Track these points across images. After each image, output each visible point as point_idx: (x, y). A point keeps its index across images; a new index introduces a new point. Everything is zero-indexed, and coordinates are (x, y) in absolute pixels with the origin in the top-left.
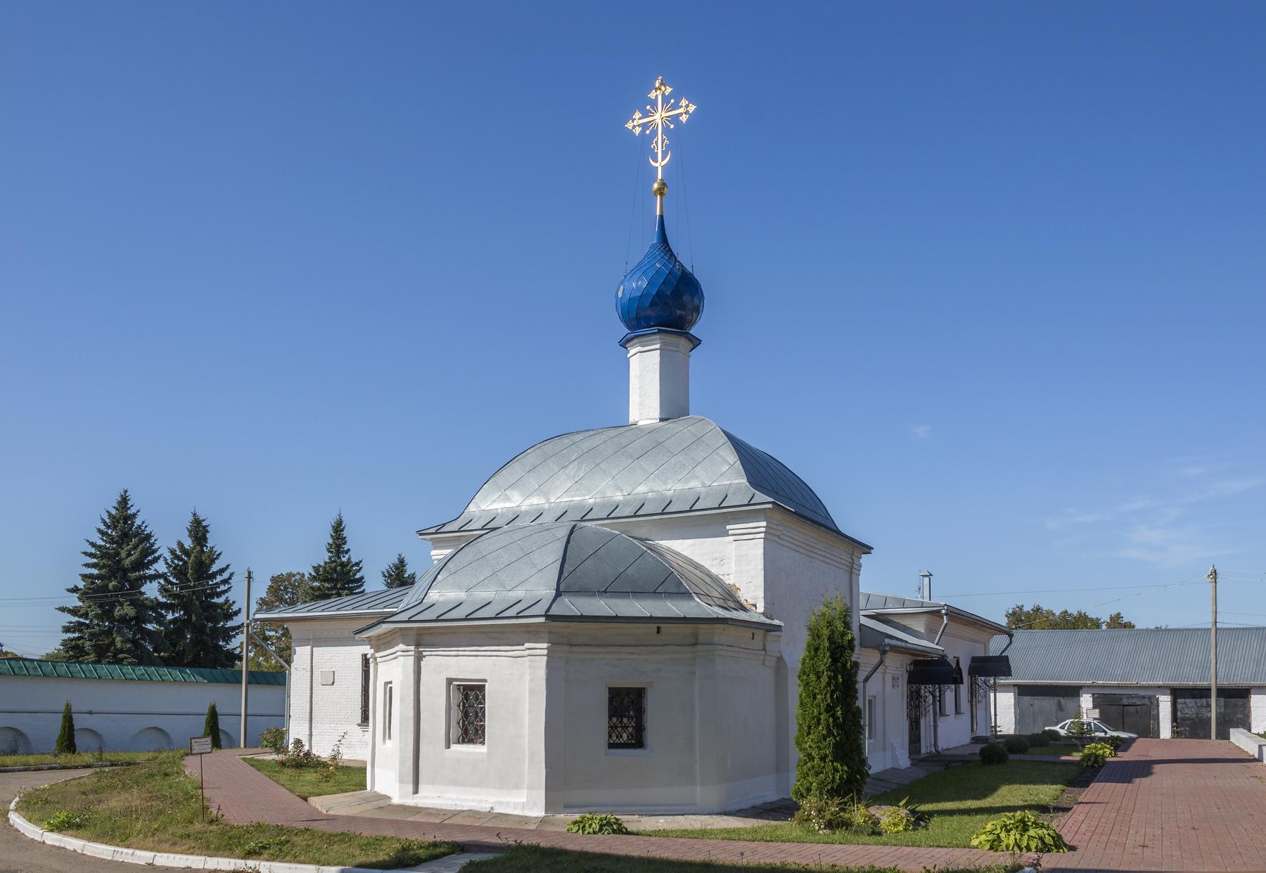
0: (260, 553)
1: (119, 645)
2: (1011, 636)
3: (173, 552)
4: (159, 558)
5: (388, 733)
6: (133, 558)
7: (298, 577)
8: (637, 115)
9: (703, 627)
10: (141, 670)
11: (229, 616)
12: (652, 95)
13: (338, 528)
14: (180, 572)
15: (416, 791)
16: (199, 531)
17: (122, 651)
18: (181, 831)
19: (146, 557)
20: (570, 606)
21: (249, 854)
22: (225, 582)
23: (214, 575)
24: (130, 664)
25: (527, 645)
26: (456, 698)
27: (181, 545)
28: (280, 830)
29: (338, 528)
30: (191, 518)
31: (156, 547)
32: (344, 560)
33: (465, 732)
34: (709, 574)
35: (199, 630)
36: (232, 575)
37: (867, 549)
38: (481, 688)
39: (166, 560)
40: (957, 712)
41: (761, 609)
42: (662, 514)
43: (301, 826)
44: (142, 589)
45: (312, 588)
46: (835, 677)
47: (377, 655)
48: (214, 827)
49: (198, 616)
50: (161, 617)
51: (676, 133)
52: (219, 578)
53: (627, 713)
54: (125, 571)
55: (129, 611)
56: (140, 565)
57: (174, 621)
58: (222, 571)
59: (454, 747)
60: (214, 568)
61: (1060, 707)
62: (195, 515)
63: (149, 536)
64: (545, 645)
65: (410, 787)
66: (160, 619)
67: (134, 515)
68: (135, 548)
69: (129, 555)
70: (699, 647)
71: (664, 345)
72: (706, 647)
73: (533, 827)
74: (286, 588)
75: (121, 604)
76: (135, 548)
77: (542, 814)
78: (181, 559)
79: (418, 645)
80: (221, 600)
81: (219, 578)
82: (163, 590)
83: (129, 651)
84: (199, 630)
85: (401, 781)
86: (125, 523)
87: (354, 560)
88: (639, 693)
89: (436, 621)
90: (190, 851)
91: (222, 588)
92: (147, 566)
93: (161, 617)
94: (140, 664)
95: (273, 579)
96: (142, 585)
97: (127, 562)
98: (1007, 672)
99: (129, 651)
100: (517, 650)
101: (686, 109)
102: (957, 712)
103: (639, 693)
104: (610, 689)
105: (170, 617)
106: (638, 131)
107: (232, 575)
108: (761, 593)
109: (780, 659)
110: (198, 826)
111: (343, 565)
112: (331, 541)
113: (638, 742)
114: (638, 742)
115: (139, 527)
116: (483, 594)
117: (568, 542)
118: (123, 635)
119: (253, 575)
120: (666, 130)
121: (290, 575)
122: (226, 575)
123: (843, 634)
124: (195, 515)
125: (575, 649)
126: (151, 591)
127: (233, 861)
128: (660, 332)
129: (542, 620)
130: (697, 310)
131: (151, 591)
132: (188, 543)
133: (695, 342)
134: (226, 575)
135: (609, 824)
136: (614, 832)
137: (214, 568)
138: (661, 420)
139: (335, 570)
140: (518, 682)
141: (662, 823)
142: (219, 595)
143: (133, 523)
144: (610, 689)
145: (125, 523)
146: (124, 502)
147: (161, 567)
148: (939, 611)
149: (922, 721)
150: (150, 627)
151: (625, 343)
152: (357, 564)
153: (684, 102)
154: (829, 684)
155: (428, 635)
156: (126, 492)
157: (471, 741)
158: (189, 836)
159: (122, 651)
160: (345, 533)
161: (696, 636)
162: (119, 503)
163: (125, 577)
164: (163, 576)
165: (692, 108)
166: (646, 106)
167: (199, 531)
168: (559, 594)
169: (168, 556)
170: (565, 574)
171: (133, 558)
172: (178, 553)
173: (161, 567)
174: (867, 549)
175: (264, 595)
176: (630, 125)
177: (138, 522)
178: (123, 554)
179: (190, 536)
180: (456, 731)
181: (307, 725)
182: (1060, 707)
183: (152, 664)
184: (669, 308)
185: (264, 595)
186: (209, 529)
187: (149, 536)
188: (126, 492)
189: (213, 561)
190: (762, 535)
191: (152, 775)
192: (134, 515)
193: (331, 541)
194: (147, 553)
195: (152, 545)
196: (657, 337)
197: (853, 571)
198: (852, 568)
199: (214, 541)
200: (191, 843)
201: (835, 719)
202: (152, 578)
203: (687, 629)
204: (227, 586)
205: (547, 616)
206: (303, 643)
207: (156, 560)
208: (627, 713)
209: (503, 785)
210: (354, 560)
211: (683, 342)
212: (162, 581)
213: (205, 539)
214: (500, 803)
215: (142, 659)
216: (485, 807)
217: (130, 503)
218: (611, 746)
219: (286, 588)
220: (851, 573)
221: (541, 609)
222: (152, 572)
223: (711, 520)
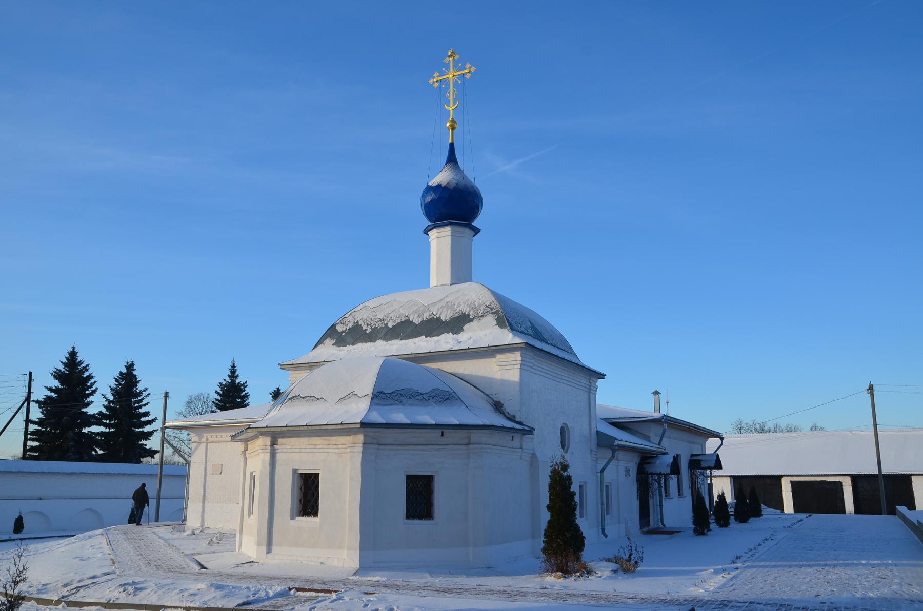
0: (172, 393)
2: (722, 439)
5: (251, 512)
8: (436, 75)
12: (447, 60)
13: (233, 367)
15: (269, 551)
20: (376, 418)
26: (299, 483)
29: (233, 367)
37: (601, 376)
40: (680, 492)
50: (89, 430)
51: (463, 84)
65: (264, 549)
70: (471, 446)
72: (476, 446)
77: (345, 552)
85: (259, 544)
93: (89, 430)
98: (718, 465)
101: (468, 70)
102: (680, 492)
106: (436, 85)
109: (534, 456)
120: (455, 84)
128: (450, 224)
133: (476, 231)
149: (651, 502)
151: (426, 232)
153: (468, 66)
165: (473, 69)
166: (442, 68)
174: (601, 376)
176: (431, 81)
184: (454, 206)
190: (519, 366)
197: (591, 391)
198: (590, 389)
203: (463, 433)
211: (467, 231)
220: (589, 392)
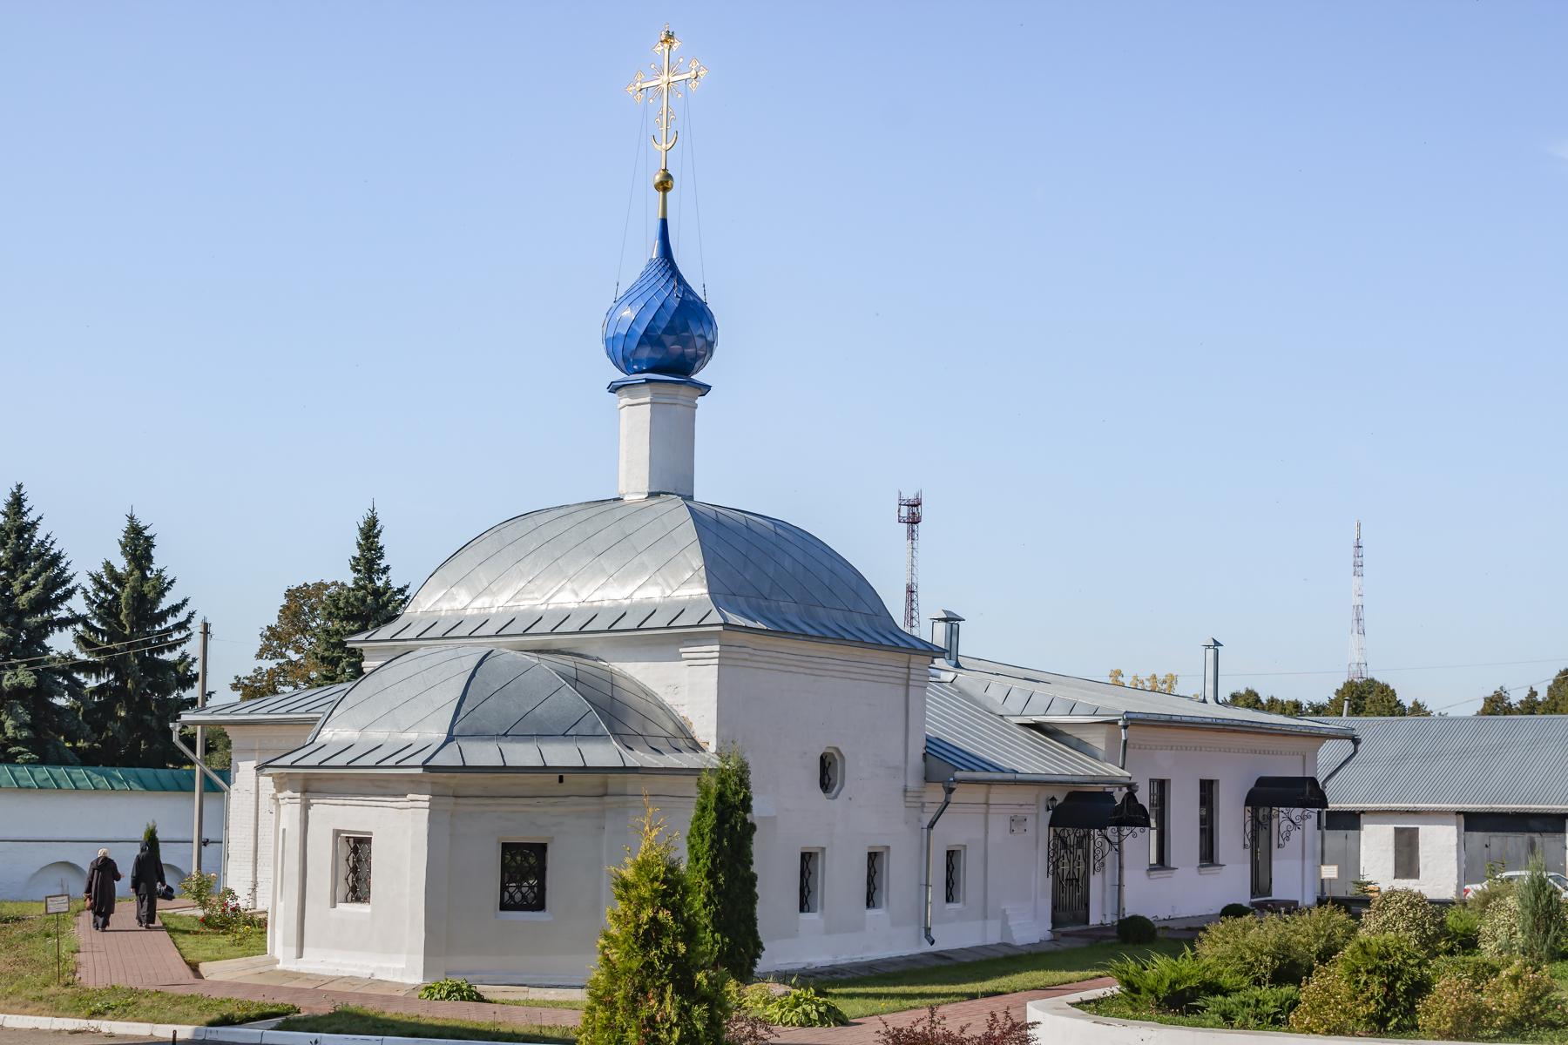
1: (10, 733)
3: (97, 580)
4: (73, 591)
6: (32, 594)
7: (333, 590)
9: (614, 779)
10: (42, 772)
11: (188, 682)
13: (370, 532)
14: (108, 611)
15: (300, 955)
16: (138, 545)
17: (15, 742)
18: (34, 994)
19: (53, 590)
21: (94, 1014)
22: (181, 626)
23: (163, 616)
24: (28, 762)
25: (410, 796)
26: (345, 850)
27: (109, 567)
28: (133, 992)
29: (370, 532)
30: (125, 524)
31: (68, 573)
32: (380, 584)
33: (354, 889)
34: (662, 706)
35: (140, 706)
36: (191, 615)
38: (368, 841)
39: (85, 592)
40: (1208, 856)
41: (712, 748)
42: (609, 631)
43: (153, 989)
44: (47, 642)
45: (327, 631)
46: (720, 841)
47: (280, 796)
48: (69, 990)
49: (137, 684)
52: (171, 621)
53: (524, 875)
54: (21, 614)
55: (26, 678)
56: (45, 603)
57: (100, 690)
58: (175, 609)
59: (341, 906)
60: (164, 604)
61: (1532, 845)
62: (131, 518)
63: (57, 558)
64: (427, 797)
65: (294, 951)
66: (75, 689)
67: (34, 525)
68: (35, 576)
69: (27, 587)
70: (607, 799)
71: (654, 395)
73: (401, 994)
74: (313, 609)
75: (13, 667)
76: (35, 576)
78: (111, 591)
79: (305, 791)
80: (170, 656)
81: (171, 621)
82: (82, 641)
83: (24, 742)
84: (140, 706)
86: (20, 537)
87: (395, 585)
88: (541, 850)
89: (318, 767)
90: (40, 1013)
91: (176, 636)
92: (54, 604)
94: (43, 761)
95: (291, 594)
96: (46, 635)
97: (23, 601)
99: (24, 742)
100: (402, 802)
103: (541, 850)
104: (506, 847)
105: (92, 683)
107: (191, 615)
108: (713, 730)
110: (53, 989)
111: (377, 593)
112: (357, 553)
113: (537, 903)
114: (537, 903)
115: (42, 543)
116: (377, 735)
117: (473, 675)
118: (15, 716)
119: (212, 629)
121: (321, 587)
122: (182, 616)
123: (736, 793)
124: (131, 518)
125: (460, 801)
126: (61, 643)
127: (77, 1021)
129: (420, 771)
130: (710, 346)
131: (61, 643)
132: (121, 564)
133: (704, 389)
134: (182, 616)
135: (459, 990)
136: (463, 998)
137: (164, 604)
138: (651, 495)
139: (364, 600)
140: (401, 832)
141: (552, 994)
142: (172, 648)
143: (32, 537)
144: (506, 847)
145: (20, 537)
146: (17, 502)
147: (78, 604)
148: (1115, 723)
150: (60, 701)
152: (401, 591)
154: (711, 847)
155: (312, 784)
156: (20, 487)
157: (358, 900)
158: (41, 999)
159: (15, 742)
160: (381, 541)
161: (605, 785)
162: (9, 505)
163: (19, 625)
164: (82, 619)
167: (138, 545)
168: (450, 738)
169: (90, 586)
170: (462, 715)
171: (32, 594)
172: (105, 580)
173: (78, 604)
175: (274, 622)
177: (39, 535)
178: (17, 588)
179: (124, 553)
180: (343, 889)
181: (250, 868)
182: (1532, 845)
183: (62, 761)
185: (274, 622)
186: (155, 541)
187: (57, 558)
188: (20, 487)
189: (161, 594)
191: (30, 936)
192: (34, 525)
193: (357, 553)
194: (56, 584)
195: (63, 571)
196: (647, 387)
199: (160, 560)
200: (42, 1005)
201: (717, 886)
202: (63, 623)
204: (184, 634)
205: (425, 767)
206: (248, 753)
207: (69, 594)
208: (524, 875)
209: (377, 950)
210: (395, 585)
212: (80, 627)
213: (149, 559)
214: (381, 969)
215: (46, 755)
216: (364, 973)
217: (27, 505)
218: (504, 907)
219: (313, 609)
221: (418, 760)
222: (63, 613)
223: (664, 637)
